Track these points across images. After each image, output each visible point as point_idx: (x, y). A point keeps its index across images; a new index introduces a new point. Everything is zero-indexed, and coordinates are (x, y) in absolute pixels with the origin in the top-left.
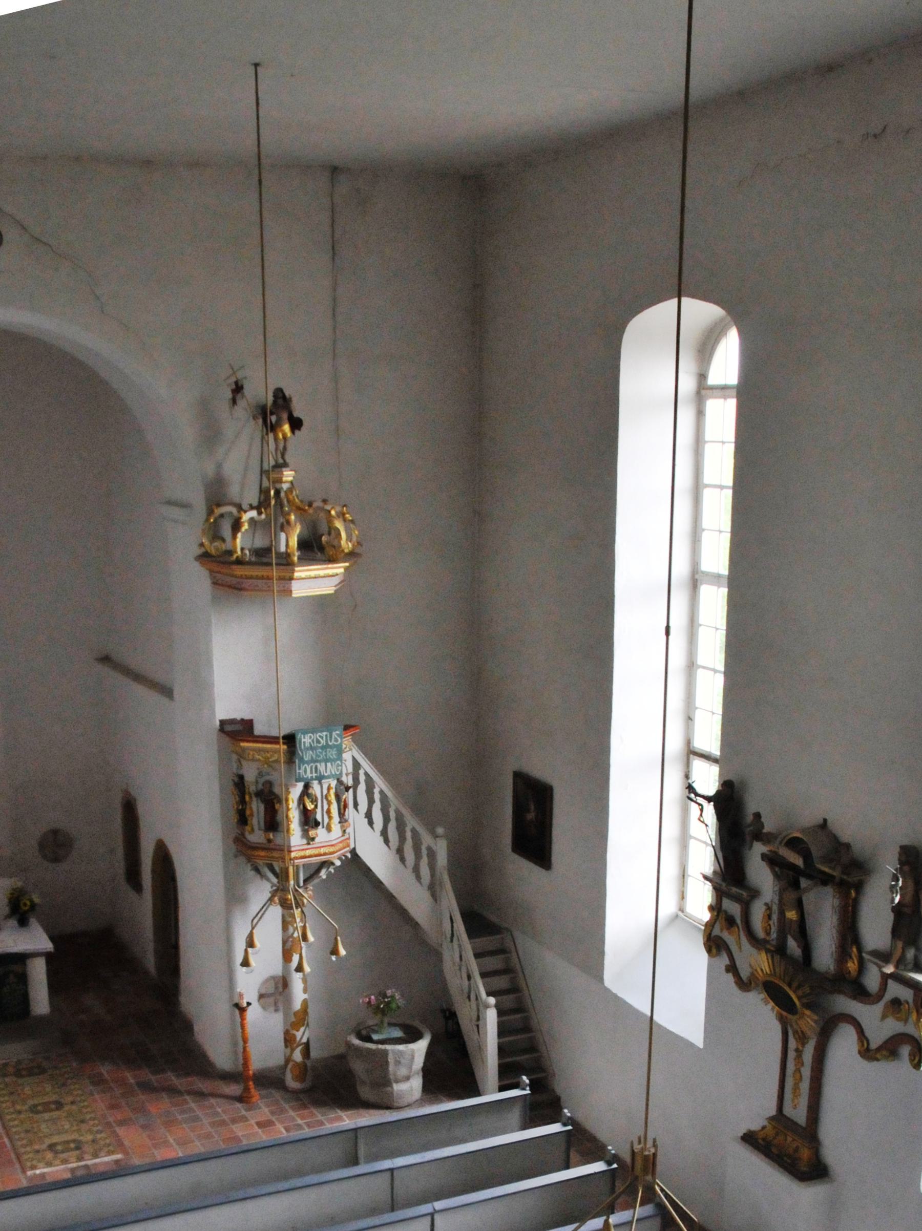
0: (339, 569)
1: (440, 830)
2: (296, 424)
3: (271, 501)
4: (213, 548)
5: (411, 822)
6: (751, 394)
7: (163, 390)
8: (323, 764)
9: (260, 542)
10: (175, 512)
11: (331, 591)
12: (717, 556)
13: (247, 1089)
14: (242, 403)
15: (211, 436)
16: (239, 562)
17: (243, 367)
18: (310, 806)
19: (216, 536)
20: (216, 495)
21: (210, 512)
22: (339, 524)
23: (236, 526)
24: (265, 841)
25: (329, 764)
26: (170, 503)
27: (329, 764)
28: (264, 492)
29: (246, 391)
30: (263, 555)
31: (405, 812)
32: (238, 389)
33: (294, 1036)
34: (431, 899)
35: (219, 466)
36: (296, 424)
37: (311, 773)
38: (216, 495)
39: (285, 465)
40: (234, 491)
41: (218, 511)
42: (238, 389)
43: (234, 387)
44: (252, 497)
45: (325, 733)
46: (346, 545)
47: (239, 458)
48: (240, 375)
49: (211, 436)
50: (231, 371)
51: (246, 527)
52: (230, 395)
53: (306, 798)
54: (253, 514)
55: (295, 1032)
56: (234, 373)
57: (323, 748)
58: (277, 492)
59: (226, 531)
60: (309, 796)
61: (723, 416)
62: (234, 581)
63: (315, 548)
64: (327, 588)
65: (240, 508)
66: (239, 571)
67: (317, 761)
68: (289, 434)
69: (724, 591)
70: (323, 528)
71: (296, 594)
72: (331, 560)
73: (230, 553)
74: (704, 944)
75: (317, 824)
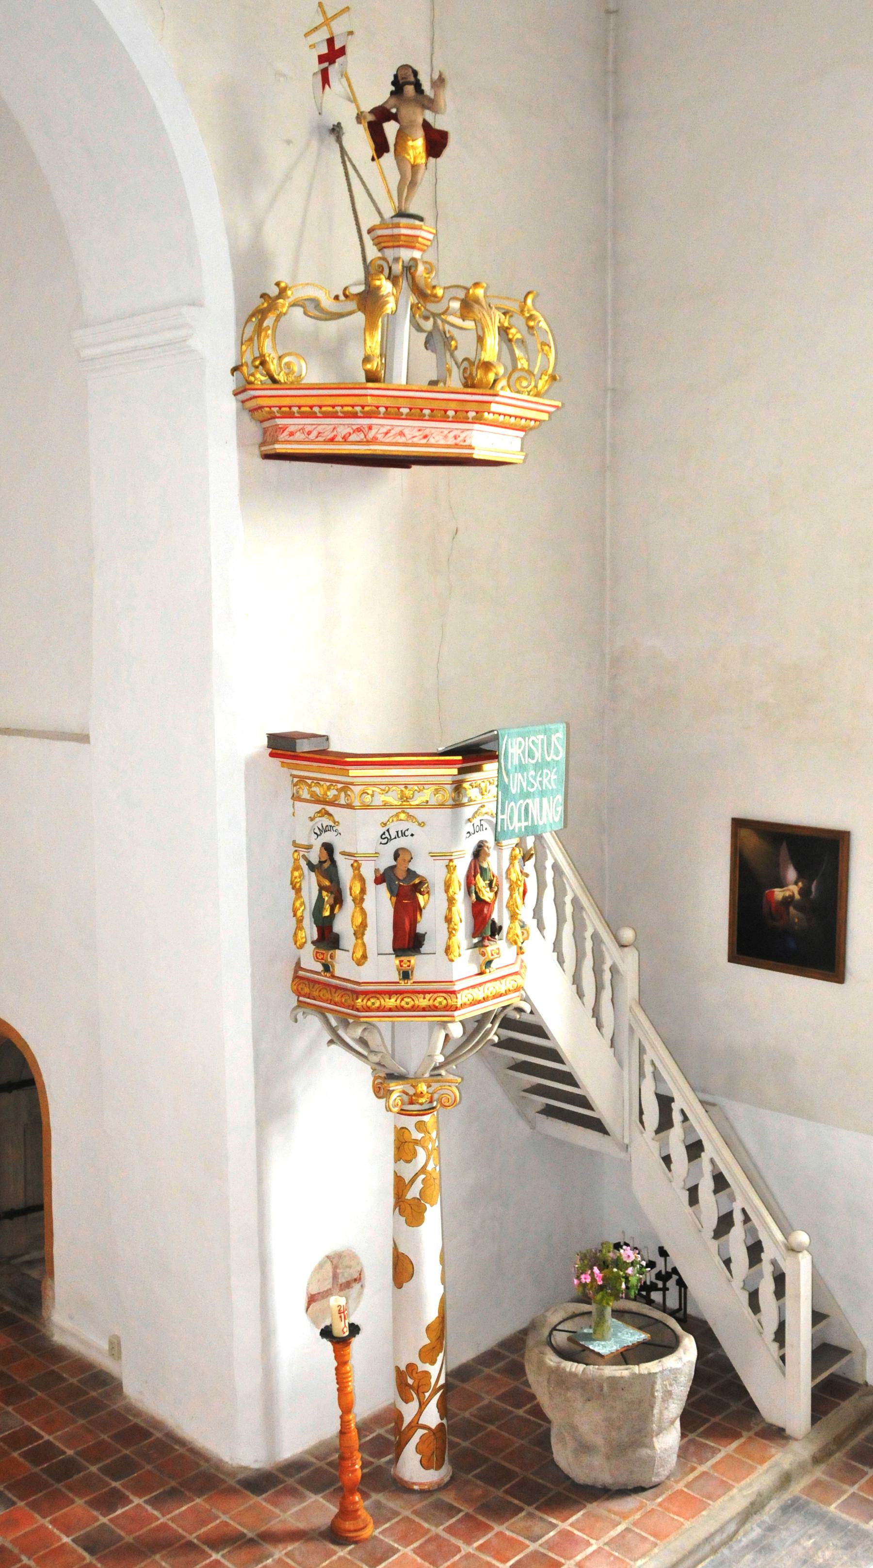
1: (800, 884)
2: (436, 143)
5: (593, 923)
8: (537, 800)
13: (346, 1512)
17: (348, 8)
18: (487, 895)
24: (395, 977)
25: (545, 800)
27: (545, 800)
31: (585, 901)
33: (427, 1374)
34: (614, 1061)
35: (258, 228)
37: (519, 820)
43: (324, 50)
45: (541, 737)
48: (339, 28)
50: (320, 19)
52: (316, 67)
55: (427, 1367)
56: (327, 22)
57: (538, 767)
60: (484, 872)
67: (528, 795)
68: (422, 160)
74: (51, 1274)
75: (496, 930)
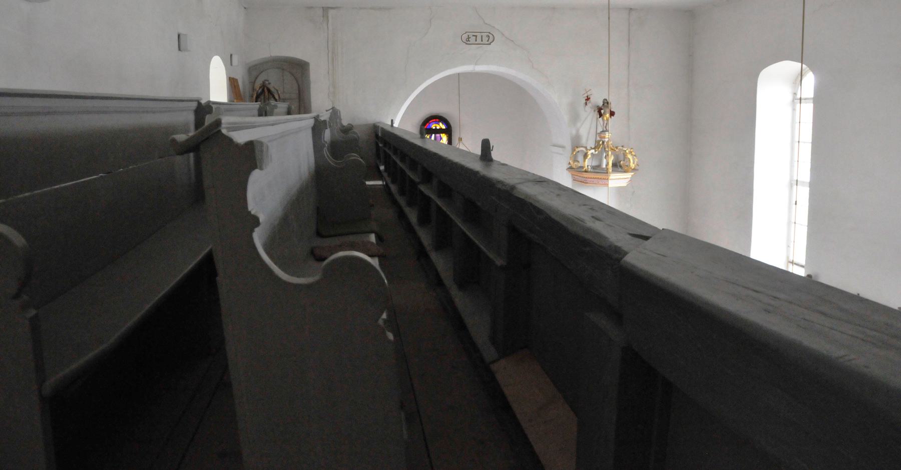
0: (629, 175)
3: (599, 145)
4: (574, 165)
6: (818, 100)
7: (556, 98)
9: (595, 163)
10: (560, 150)
11: (625, 185)
12: (805, 175)
14: (589, 105)
15: (575, 118)
16: (586, 171)
19: (575, 160)
20: (576, 143)
21: (574, 150)
22: (629, 156)
23: (586, 156)
26: (554, 146)
28: (597, 142)
29: (591, 99)
30: (597, 169)
32: (588, 99)
35: (578, 131)
36: (612, 114)
38: (576, 143)
39: (607, 131)
40: (583, 141)
41: (577, 150)
42: (588, 99)
44: (591, 144)
46: (632, 166)
47: (588, 126)
48: (589, 93)
49: (575, 118)
51: (590, 156)
53: (444, 127)
54: (593, 151)
58: (603, 142)
59: (580, 158)
61: (807, 110)
62: (583, 179)
63: (617, 166)
64: (624, 183)
65: (586, 148)
66: (586, 175)
69: (808, 189)
70: (621, 158)
71: (610, 186)
72: (625, 172)
73: (582, 167)
